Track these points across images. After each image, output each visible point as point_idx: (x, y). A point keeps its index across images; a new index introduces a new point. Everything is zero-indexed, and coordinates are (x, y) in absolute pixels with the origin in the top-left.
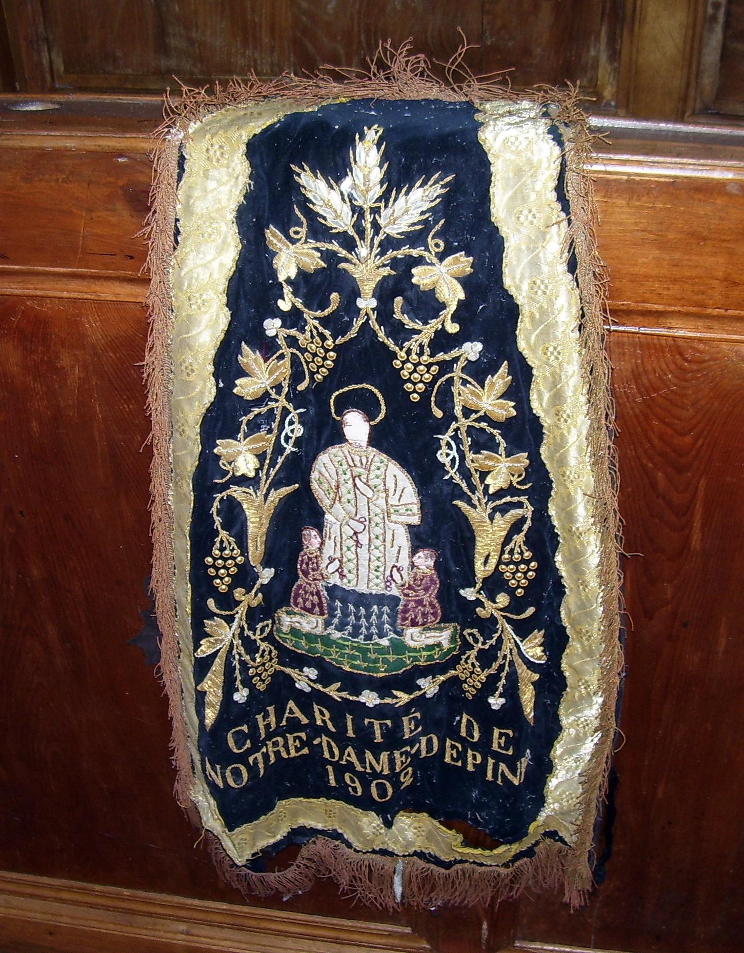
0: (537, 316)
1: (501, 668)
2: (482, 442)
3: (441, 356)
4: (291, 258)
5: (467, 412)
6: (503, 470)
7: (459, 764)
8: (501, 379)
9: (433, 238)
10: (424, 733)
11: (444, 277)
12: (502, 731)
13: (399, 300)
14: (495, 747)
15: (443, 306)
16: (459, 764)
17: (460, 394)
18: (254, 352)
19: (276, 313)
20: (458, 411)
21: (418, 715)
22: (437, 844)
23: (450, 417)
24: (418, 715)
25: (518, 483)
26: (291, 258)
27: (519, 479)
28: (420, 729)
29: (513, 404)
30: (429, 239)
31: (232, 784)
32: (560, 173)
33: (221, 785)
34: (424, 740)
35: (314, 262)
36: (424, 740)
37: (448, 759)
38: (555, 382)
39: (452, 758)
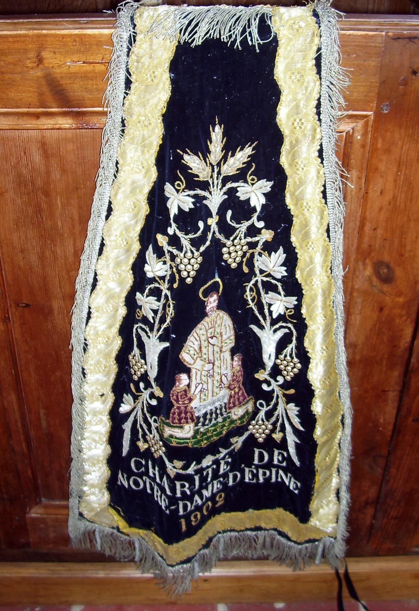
0: (294, 143)
1: (277, 420)
2: (269, 287)
3: (249, 239)
4: (178, 200)
5: (262, 272)
6: (279, 304)
7: (255, 481)
8: (280, 256)
9: (250, 176)
10: (231, 471)
11: (255, 193)
12: (280, 451)
13: (229, 213)
14: (276, 462)
15: (254, 209)
16: (255, 481)
17: (258, 261)
18: (154, 254)
19: (165, 233)
20: (257, 272)
21: (230, 460)
22: (292, 132)
23: (252, 273)
24: (230, 460)
25: (289, 316)
26: (178, 200)
27: (289, 314)
28: (228, 468)
29: (285, 268)
30: (248, 177)
31: (133, 487)
32: (71, 13)
33: (127, 486)
34: (231, 476)
35: (188, 204)
36: (231, 476)
37: (247, 480)
38: (306, 225)
39: (250, 479)
